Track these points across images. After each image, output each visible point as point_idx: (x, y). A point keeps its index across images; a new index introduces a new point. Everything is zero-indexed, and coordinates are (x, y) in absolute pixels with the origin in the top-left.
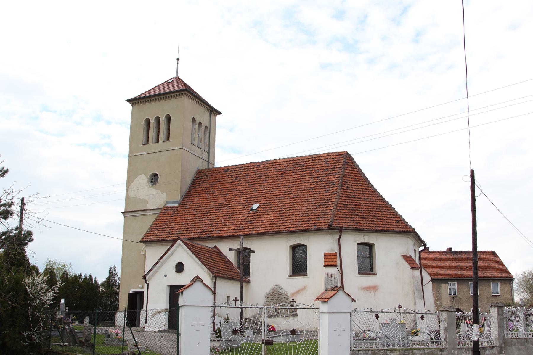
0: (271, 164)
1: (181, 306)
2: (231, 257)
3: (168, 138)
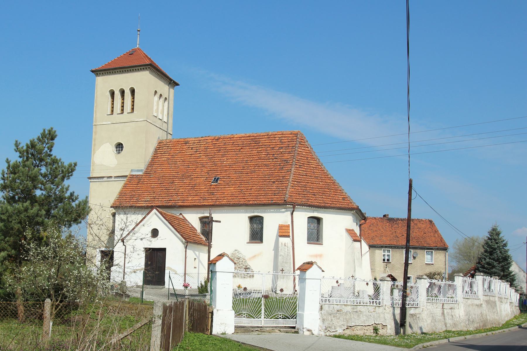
0: (229, 139)
2: (197, 225)
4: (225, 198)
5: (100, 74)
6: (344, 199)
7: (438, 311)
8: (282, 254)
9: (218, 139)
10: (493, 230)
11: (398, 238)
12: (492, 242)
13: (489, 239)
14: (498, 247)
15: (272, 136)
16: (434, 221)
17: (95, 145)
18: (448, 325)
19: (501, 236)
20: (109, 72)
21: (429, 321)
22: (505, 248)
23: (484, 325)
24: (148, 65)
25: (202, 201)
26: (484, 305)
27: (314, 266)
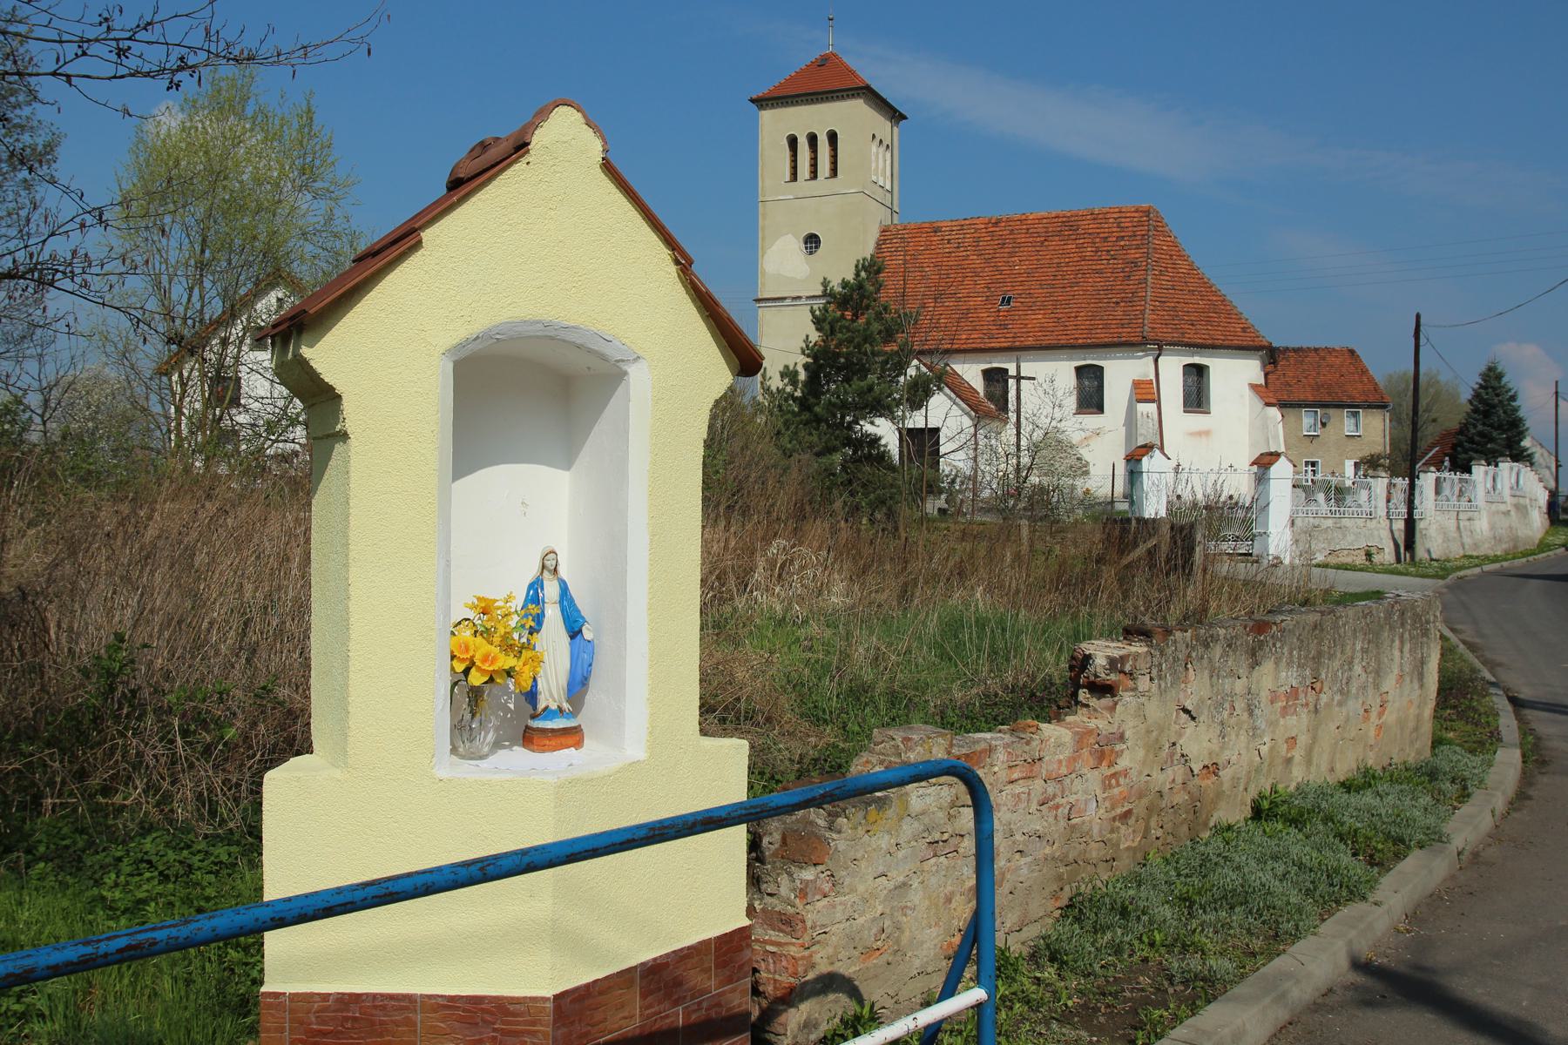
1: (1129, 497)
2: (978, 383)
3: (834, 172)
4: (1031, 334)
5: (767, 105)
6: (1244, 330)
7: (1452, 524)
8: (1143, 432)
9: (996, 223)
10: (1490, 369)
11: (1290, 386)
12: (1487, 394)
13: (1481, 386)
14: (1500, 402)
15: (1100, 216)
16: (1359, 352)
17: (763, 239)
18: (1467, 547)
19: (1504, 380)
20: (784, 101)
21: (1440, 541)
22: (1514, 404)
23: (1515, 547)
24: (861, 88)
25: (987, 341)
26: (1513, 513)
27: (1282, 459)
